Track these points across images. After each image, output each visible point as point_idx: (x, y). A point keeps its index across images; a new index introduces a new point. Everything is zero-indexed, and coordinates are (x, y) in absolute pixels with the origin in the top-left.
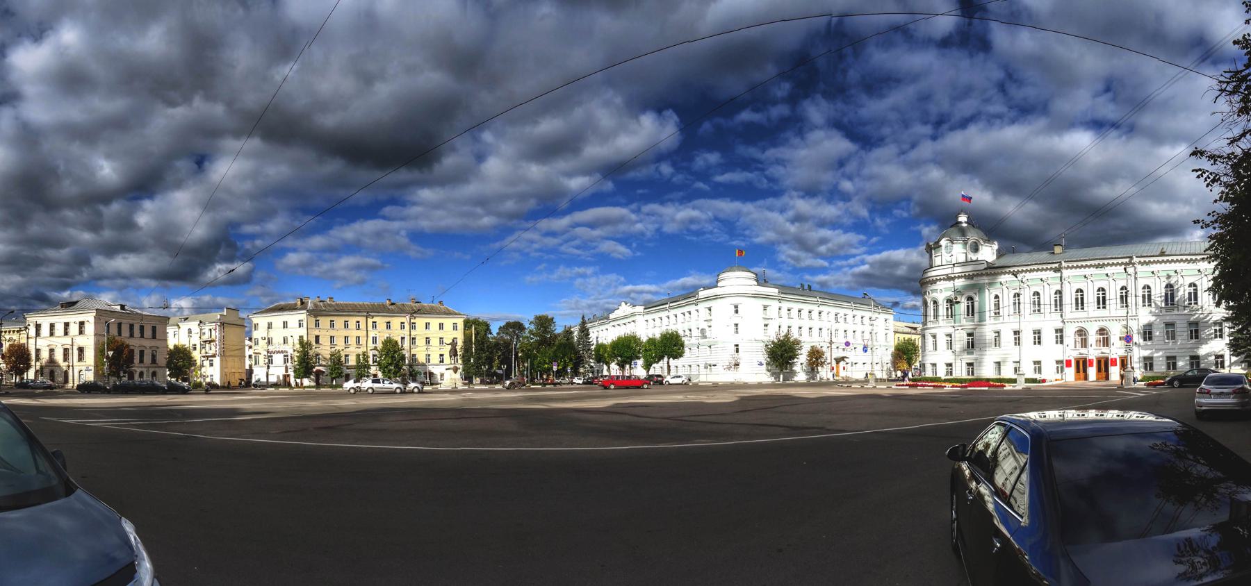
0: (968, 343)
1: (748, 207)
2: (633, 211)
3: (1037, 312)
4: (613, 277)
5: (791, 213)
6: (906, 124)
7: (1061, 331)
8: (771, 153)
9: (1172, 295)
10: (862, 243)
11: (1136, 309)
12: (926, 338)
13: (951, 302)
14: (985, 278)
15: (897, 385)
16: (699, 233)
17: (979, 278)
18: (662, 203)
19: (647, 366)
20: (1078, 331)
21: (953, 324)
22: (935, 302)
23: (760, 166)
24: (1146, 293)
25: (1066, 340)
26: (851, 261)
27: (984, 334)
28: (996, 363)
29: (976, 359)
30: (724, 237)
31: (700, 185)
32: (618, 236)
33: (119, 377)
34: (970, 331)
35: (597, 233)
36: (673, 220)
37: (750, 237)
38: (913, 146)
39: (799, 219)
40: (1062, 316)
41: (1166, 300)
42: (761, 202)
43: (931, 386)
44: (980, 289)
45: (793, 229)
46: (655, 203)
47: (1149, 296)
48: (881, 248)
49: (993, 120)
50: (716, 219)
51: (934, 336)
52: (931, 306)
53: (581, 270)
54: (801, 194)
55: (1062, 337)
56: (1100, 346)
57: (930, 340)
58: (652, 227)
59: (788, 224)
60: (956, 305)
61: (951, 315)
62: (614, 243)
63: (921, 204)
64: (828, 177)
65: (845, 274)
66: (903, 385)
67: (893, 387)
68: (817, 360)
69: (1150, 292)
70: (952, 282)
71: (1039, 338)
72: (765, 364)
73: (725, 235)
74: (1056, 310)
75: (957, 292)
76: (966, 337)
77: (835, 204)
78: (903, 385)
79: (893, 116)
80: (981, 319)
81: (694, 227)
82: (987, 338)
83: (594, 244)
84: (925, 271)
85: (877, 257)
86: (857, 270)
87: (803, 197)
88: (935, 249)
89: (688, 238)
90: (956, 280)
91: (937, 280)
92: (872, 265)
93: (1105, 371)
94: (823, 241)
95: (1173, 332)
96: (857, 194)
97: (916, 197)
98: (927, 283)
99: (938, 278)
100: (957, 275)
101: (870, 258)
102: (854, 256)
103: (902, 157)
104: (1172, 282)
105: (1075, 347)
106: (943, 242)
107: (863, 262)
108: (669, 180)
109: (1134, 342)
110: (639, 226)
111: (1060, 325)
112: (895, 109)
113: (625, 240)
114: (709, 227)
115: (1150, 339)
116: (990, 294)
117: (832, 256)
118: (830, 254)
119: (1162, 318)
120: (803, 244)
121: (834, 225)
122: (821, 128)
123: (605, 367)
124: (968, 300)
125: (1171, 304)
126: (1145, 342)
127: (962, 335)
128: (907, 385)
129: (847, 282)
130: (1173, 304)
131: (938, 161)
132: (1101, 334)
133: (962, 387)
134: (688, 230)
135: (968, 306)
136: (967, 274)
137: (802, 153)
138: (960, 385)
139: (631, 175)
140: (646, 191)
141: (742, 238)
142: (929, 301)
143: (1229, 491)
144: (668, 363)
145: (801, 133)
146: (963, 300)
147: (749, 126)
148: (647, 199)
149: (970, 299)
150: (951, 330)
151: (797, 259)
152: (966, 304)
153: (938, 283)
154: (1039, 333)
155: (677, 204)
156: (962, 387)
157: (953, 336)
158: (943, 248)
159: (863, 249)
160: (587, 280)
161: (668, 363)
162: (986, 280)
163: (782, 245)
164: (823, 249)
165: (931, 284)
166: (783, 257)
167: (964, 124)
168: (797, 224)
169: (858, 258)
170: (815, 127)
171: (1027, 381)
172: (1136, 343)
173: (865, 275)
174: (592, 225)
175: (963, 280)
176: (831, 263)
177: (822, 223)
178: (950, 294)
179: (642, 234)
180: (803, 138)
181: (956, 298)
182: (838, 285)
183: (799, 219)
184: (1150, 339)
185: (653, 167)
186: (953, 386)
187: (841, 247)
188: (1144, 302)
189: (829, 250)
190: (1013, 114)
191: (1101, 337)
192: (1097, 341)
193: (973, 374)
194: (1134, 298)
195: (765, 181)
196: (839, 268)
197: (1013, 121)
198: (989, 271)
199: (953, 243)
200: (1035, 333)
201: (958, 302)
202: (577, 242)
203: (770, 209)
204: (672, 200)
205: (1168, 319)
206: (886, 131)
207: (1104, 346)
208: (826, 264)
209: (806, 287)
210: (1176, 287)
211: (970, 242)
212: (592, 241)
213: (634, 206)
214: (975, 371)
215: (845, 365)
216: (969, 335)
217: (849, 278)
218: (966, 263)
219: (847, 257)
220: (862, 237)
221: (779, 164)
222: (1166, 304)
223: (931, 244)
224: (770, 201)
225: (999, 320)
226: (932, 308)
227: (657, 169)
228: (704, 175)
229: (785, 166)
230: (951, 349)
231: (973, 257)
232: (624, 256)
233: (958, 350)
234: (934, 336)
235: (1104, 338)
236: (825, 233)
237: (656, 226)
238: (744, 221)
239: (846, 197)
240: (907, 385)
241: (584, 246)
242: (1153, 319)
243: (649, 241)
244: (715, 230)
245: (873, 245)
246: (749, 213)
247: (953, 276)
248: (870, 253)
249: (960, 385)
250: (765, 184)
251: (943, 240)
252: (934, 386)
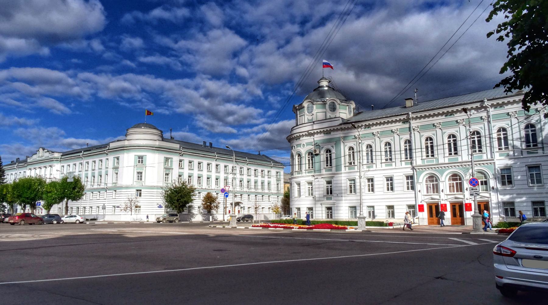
0: (327, 189)
1: (169, 84)
2: (71, 77)
3: (389, 161)
5: (203, 91)
6: (280, 24)
7: (412, 177)
8: (182, 43)
9: (534, 136)
10: (262, 116)
11: (492, 153)
12: (293, 185)
13: (312, 155)
14: (340, 132)
15: (253, 226)
16: (131, 101)
17: (335, 133)
18: (97, 73)
20: (429, 177)
21: (313, 174)
22: (299, 155)
23: (174, 53)
24: (502, 136)
25: (418, 187)
26: (255, 129)
27: (339, 182)
28: (351, 207)
29: (334, 204)
30: (150, 106)
31: (128, 62)
32: (57, 95)
33: (33, 207)
34: (328, 180)
35: (36, 89)
36: (107, 88)
37: (173, 108)
38: (288, 41)
39: (208, 95)
40: (411, 163)
41: (527, 141)
42: (179, 81)
43: (282, 227)
44: (336, 142)
45: (206, 103)
46: (91, 72)
47: (506, 139)
49: (344, 16)
50: (143, 91)
51: (299, 184)
52: (296, 158)
54: (209, 77)
55: (412, 183)
56: (454, 191)
57: (296, 187)
58: (88, 91)
59: (202, 99)
60: (316, 157)
61: (312, 163)
62: (53, 100)
63: (300, 85)
64: (228, 64)
65: (252, 138)
66: (258, 226)
67: (250, 228)
69: (506, 134)
70: (312, 137)
71: (392, 184)
74: (407, 158)
75: (317, 145)
76: (325, 185)
77: (235, 85)
78: (258, 226)
79: (269, 19)
80: (338, 168)
81: (125, 95)
82: (343, 185)
83: (33, 99)
84: (292, 129)
86: (261, 136)
87: (210, 79)
88: (299, 110)
89: (122, 104)
90: (316, 136)
91: (300, 136)
93: (460, 217)
94: (230, 113)
95: (539, 175)
96: (251, 77)
97: (297, 79)
98: (293, 139)
99: (301, 134)
100: (315, 131)
101: (268, 126)
102: (256, 125)
103: (281, 50)
104: (533, 122)
105: (428, 192)
106: (306, 104)
107: (265, 130)
108: (100, 56)
109: (491, 186)
110: (76, 90)
111: (410, 172)
112: (269, 14)
113: (64, 99)
114: (139, 96)
115: (510, 182)
116: (345, 146)
117: (239, 125)
118: (236, 123)
119: (525, 160)
120: (214, 115)
121: (237, 101)
122: (219, 28)
124: (327, 152)
125: (534, 146)
126: (504, 187)
127: (322, 183)
128: (261, 226)
129: (254, 146)
130: (536, 145)
131: (308, 51)
132: (454, 180)
133: (307, 228)
134: (121, 97)
135: (327, 158)
136: (325, 130)
137: (206, 46)
138: (308, 226)
139: (65, 45)
140: (80, 62)
142: (294, 154)
145: (203, 31)
146: (322, 152)
147: (161, 21)
148: (85, 68)
149: (328, 151)
150: (311, 179)
151: (212, 126)
152: (325, 156)
153: (301, 139)
154: (391, 180)
155: (110, 75)
156: (307, 228)
157: (314, 183)
158: (306, 108)
159: (262, 120)
162: (340, 134)
163: (199, 115)
164: (230, 119)
165: (296, 140)
166: (200, 124)
167: (323, 22)
168: (209, 99)
169: (260, 126)
170: (213, 27)
171: (368, 224)
172: (493, 188)
173: (267, 140)
174: (31, 82)
175: (322, 135)
176: (238, 131)
177: (228, 100)
178: (312, 147)
179: (80, 96)
180: (205, 35)
181: (315, 151)
182: (248, 148)
183: (208, 95)
184: (510, 182)
186: (300, 228)
187: (245, 118)
188: (500, 145)
189: (235, 120)
190: (359, 9)
191: (455, 182)
192: (450, 187)
193: (331, 217)
194: (488, 139)
195: (180, 65)
196: (247, 134)
197: (359, 16)
198: (343, 126)
199: (313, 104)
200: (388, 180)
201: (317, 155)
202: (16, 95)
203: (187, 87)
204: (106, 72)
205: (532, 161)
206: (266, 31)
207: (457, 191)
208: (234, 131)
209: (208, 144)
210: (538, 127)
211: (328, 103)
212: (31, 97)
213: (71, 72)
214: (333, 215)
215: (239, 209)
216: (329, 182)
217: (255, 142)
218: (325, 120)
219: (252, 126)
220: (260, 111)
221: (190, 53)
222: (528, 146)
223: (296, 106)
224: (186, 81)
225: (354, 169)
226: (297, 159)
227: (89, 45)
228: (131, 55)
229: (194, 56)
230: (312, 195)
231: (330, 114)
233: (317, 196)
234: (299, 184)
235: (457, 183)
236: (231, 107)
237: (93, 91)
238: (166, 95)
239: (242, 80)
240: (261, 226)
241: (25, 98)
242: (510, 162)
243: (87, 103)
244: (144, 100)
245: (269, 117)
246: (170, 90)
247: (312, 132)
249: (308, 226)
250: (179, 68)
251: (305, 102)
252: (284, 227)
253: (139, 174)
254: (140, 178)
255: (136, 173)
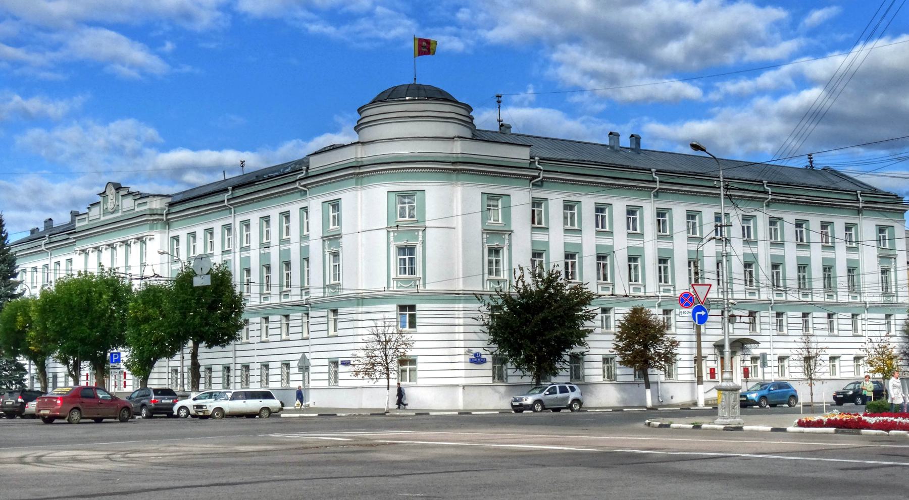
4: (127, 125)
10: (788, 30)
19: (143, 367)
26: (767, 79)
37: (472, 27)
48: (841, 38)
53: (34, 104)
62: (113, 34)
65: (762, 114)
68: (646, 347)
72: (489, 358)
73: (409, 22)
83: (56, 37)
85: (839, 61)
92: (831, 84)
101: (819, 67)
102: (773, 65)
107: (802, 82)
118: (695, 64)
123: (32, 369)
141: (453, 29)
143: (548, 369)
144: (194, 356)
159: (787, 47)
160: (57, 133)
161: (194, 356)
164: (673, 50)
169: (786, 68)
185: (713, 96)
187: (725, 42)
189: (692, 54)
208: (691, 91)
212: (48, 30)
220: (777, 13)
232: (143, 74)
245: (813, 32)
248: (818, 53)
253: (405, 255)
254: (407, 266)
255: (393, 250)
